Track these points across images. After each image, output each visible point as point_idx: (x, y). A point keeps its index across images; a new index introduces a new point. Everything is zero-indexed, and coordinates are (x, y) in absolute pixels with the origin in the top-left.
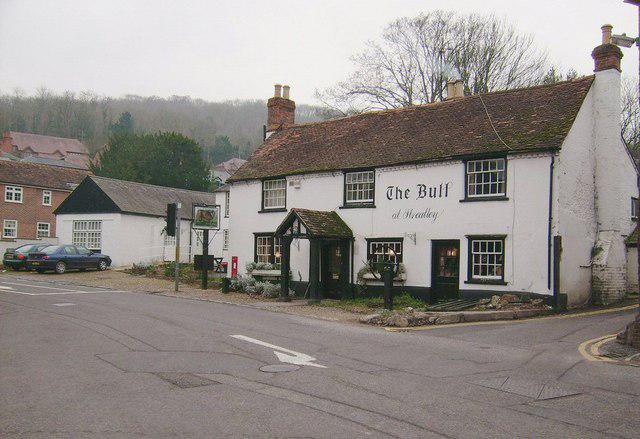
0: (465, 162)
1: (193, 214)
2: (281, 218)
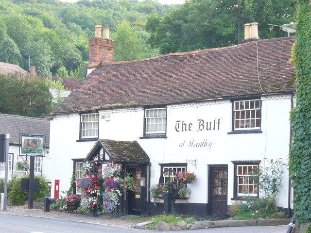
0: (232, 101)
1: (20, 140)
2: (91, 145)
